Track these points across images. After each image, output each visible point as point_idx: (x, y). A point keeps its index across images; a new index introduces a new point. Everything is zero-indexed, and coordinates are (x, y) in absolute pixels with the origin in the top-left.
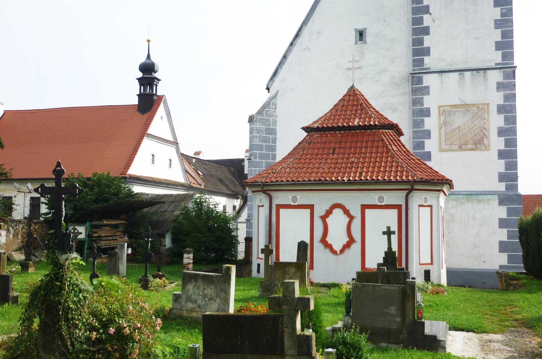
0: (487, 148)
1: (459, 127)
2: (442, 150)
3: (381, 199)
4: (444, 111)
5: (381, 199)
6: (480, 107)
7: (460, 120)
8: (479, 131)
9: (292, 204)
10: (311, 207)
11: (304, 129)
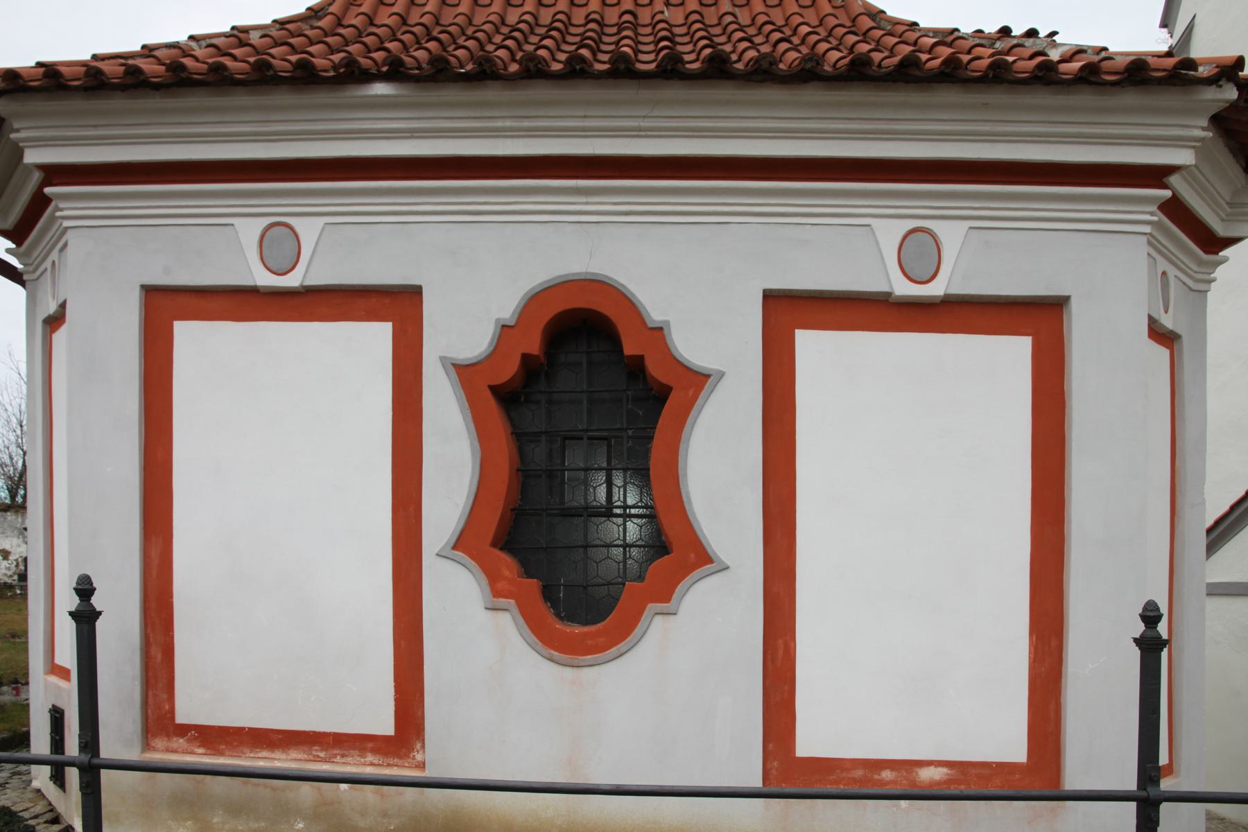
3: (919, 250)
5: (279, 243)
9: (903, 288)
10: (398, 305)
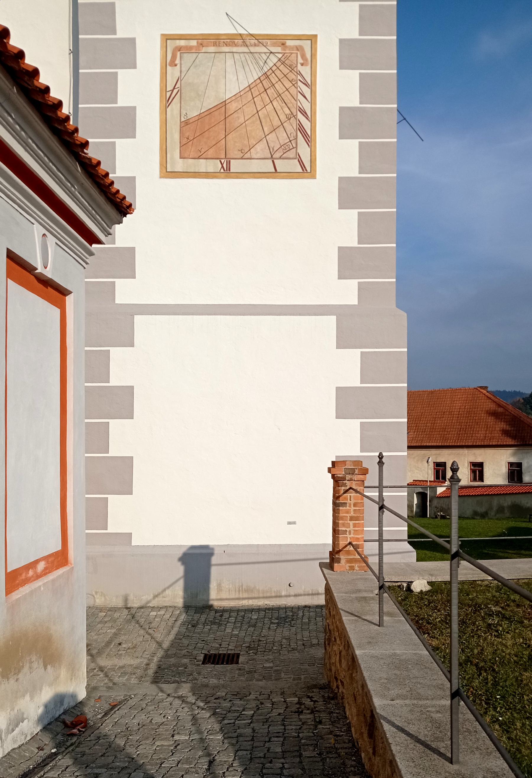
0: (307, 171)
1: (224, 103)
2: (167, 173)
4: (178, 48)
6: (289, 43)
7: (230, 79)
8: (283, 118)
11: (8, 249)
